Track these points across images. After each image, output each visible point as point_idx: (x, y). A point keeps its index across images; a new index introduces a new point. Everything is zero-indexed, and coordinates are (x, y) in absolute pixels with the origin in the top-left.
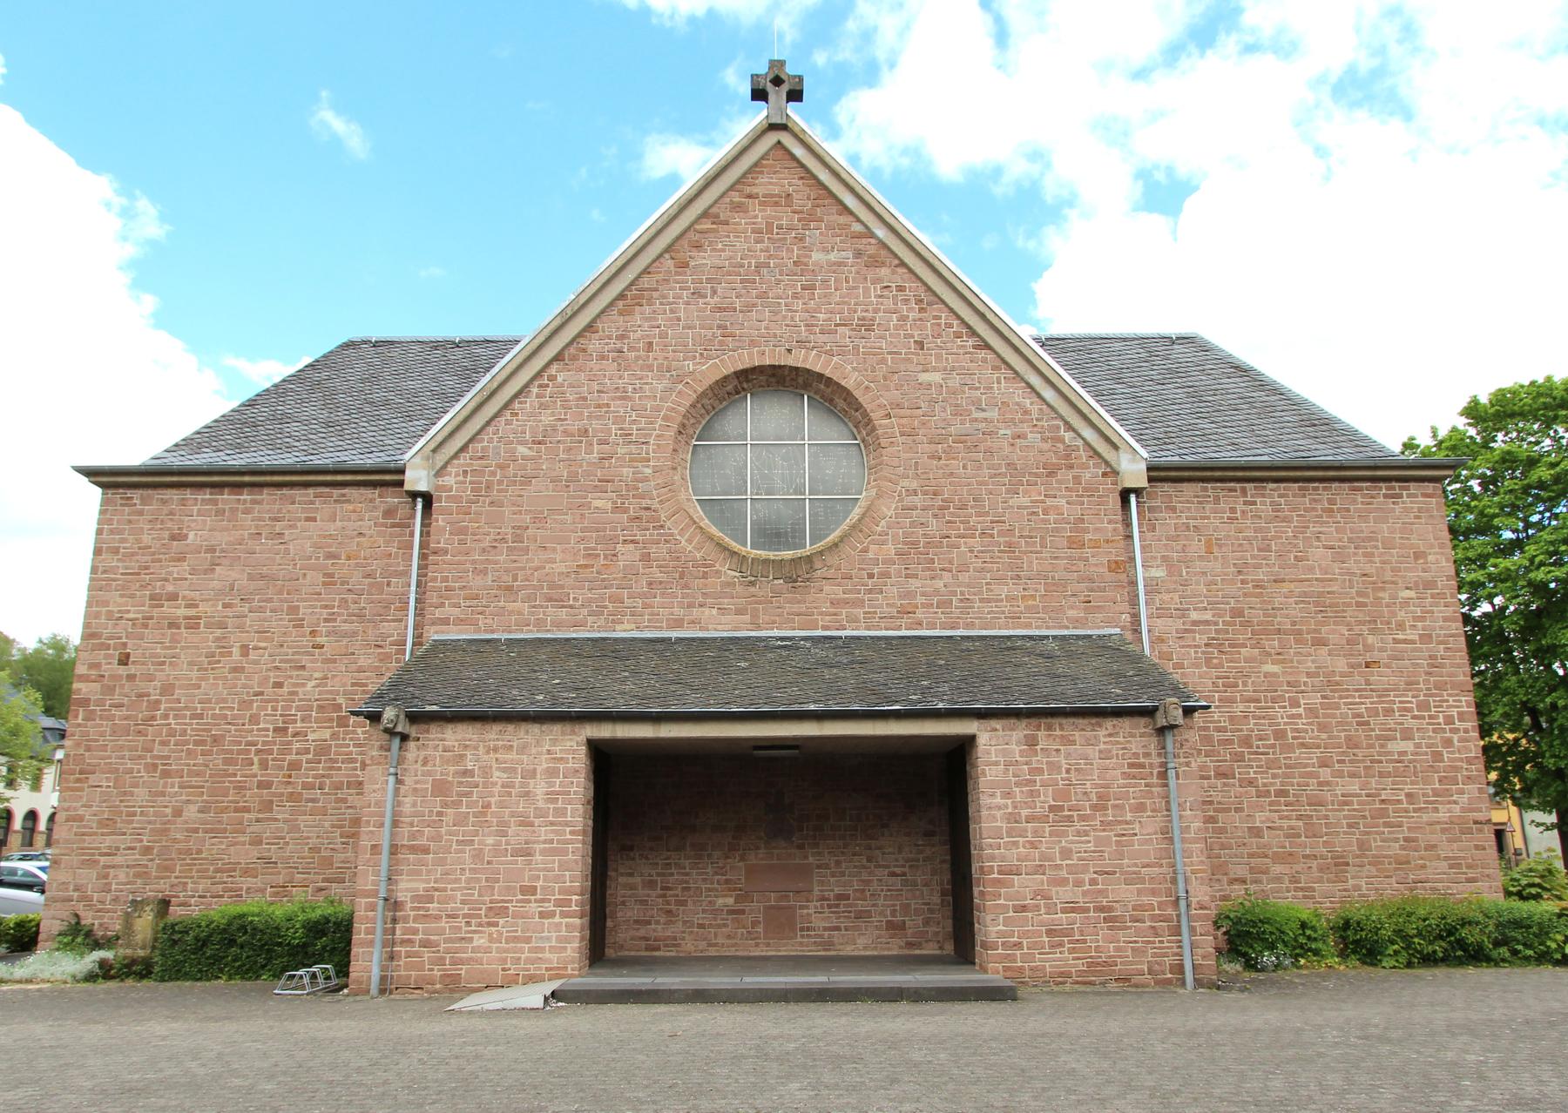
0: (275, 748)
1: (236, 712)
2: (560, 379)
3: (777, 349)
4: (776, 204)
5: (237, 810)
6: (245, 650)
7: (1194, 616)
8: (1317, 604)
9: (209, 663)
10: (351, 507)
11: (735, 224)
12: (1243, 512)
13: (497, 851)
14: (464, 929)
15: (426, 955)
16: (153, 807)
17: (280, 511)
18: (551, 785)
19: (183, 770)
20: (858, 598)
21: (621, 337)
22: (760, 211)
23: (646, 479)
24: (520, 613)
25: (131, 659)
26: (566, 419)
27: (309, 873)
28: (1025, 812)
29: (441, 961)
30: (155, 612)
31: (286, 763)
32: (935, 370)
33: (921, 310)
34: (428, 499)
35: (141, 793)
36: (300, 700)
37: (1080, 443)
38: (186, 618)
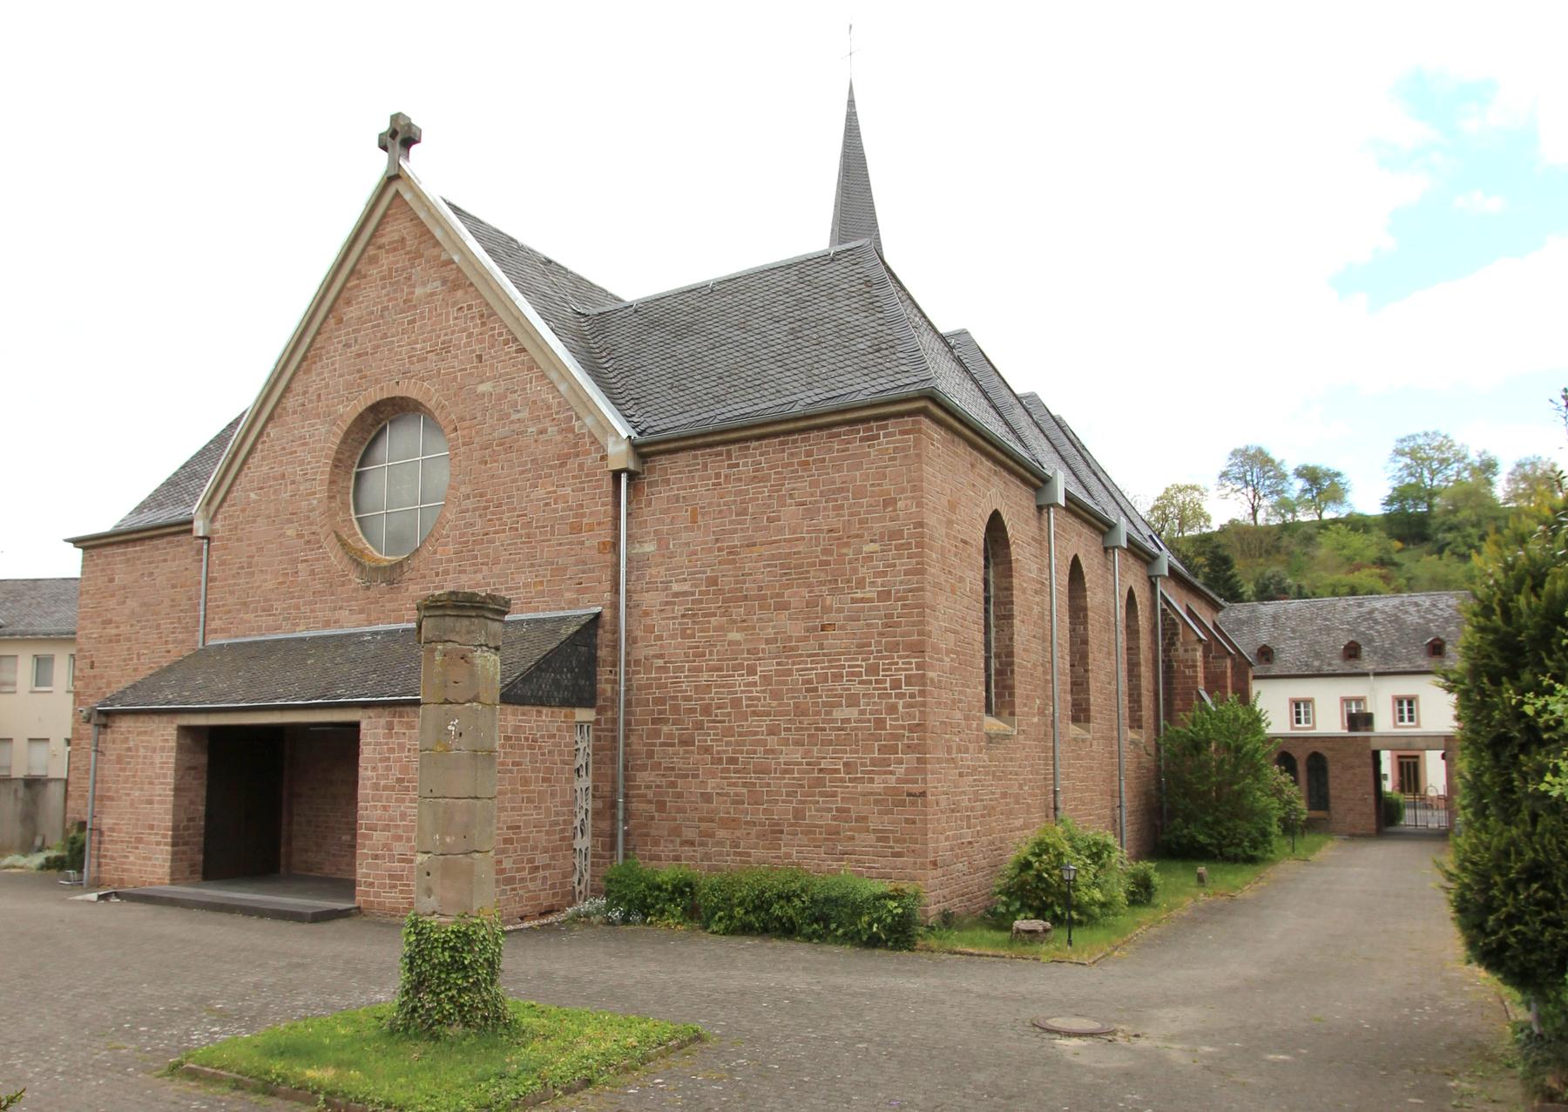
7: (676, 587)
8: (782, 566)
28: (383, 782)
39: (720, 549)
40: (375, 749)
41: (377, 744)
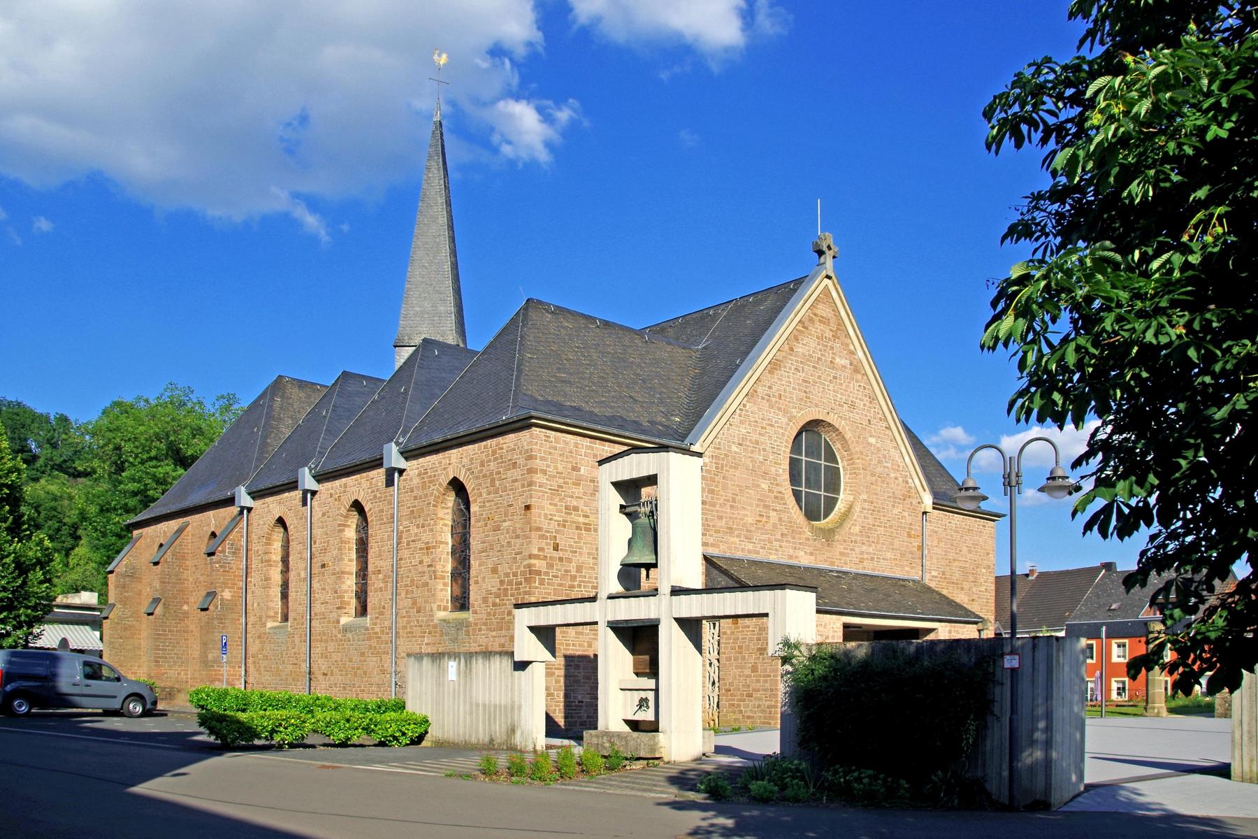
4: (824, 323)
32: (873, 436)
38: (584, 524)
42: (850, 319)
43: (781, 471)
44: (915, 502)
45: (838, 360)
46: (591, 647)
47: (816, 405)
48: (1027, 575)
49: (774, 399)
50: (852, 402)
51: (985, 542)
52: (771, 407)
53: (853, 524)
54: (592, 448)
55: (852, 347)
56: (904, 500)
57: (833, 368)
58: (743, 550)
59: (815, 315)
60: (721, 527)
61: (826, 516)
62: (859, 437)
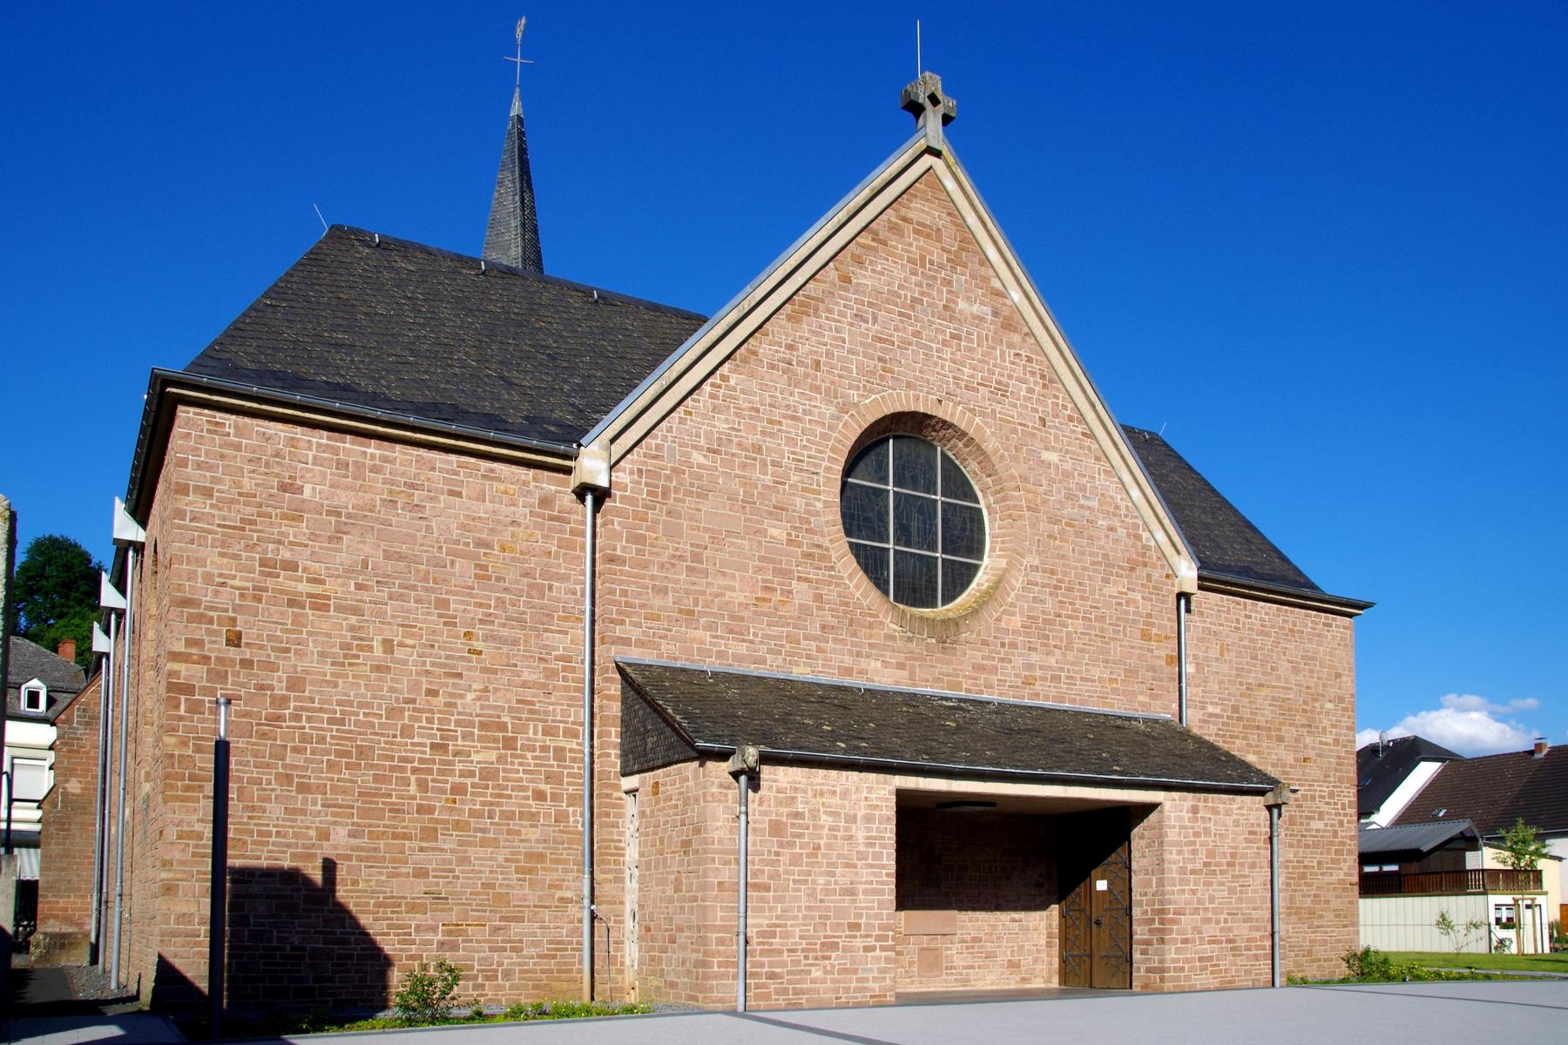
0: (435, 767)
1: (384, 720)
2: (732, 382)
3: (931, 396)
4: (928, 236)
5: (395, 836)
6: (388, 645)
7: (1211, 709)
8: (1281, 707)
9: (345, 657)
10: (502, 487)
11: (892, 246)
12: (1244, 623)
13: (827, 892)
14: (803, 962)
15: (773, 986)
16: (293, 827)
17: (417, 476)
18: (869, 830)
19: (325, 785)
20: (993, 666)
21: (790, 347)
22: (915, 239)
23: (817, 514)
24: (702, 642)
25: (243, 641)
26: (740, 430)
27: (485, 911)
28: (1190, 867)
29: (785, 991)
30: (270, 583)
31: (449, 786)
32: (1054, 449)
33: (1045, 386)
34: (601, 496)
35: (275, 810)
36: (459, 714)
37: (1153, 543)
38: (310, 595)
39: (1241, 683)
40: (1180, 833)
41: (1182, 827)
42: (988, 230)
43: (819, 505)
44: (1157, 574)
45: (962, 305)
46: (328, 839)
47: (909, 385)
48: (1531, 753)
49: (801, 370)
50: (999, 383)
51: (1332, 654)
52: (794, 382)
53: (1004, 612)
54: (336, 451)
55: (996, 284)
56: (1132, 569)
57: (951, 319)
58: (721, 655)
59: (904, 219)
60: (664, 609)
61: (948, 599)
62: (1017, 450)
